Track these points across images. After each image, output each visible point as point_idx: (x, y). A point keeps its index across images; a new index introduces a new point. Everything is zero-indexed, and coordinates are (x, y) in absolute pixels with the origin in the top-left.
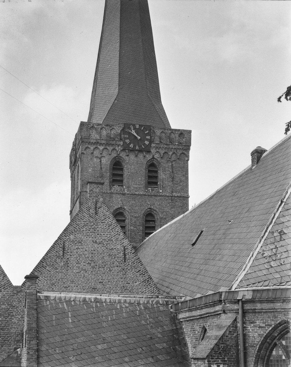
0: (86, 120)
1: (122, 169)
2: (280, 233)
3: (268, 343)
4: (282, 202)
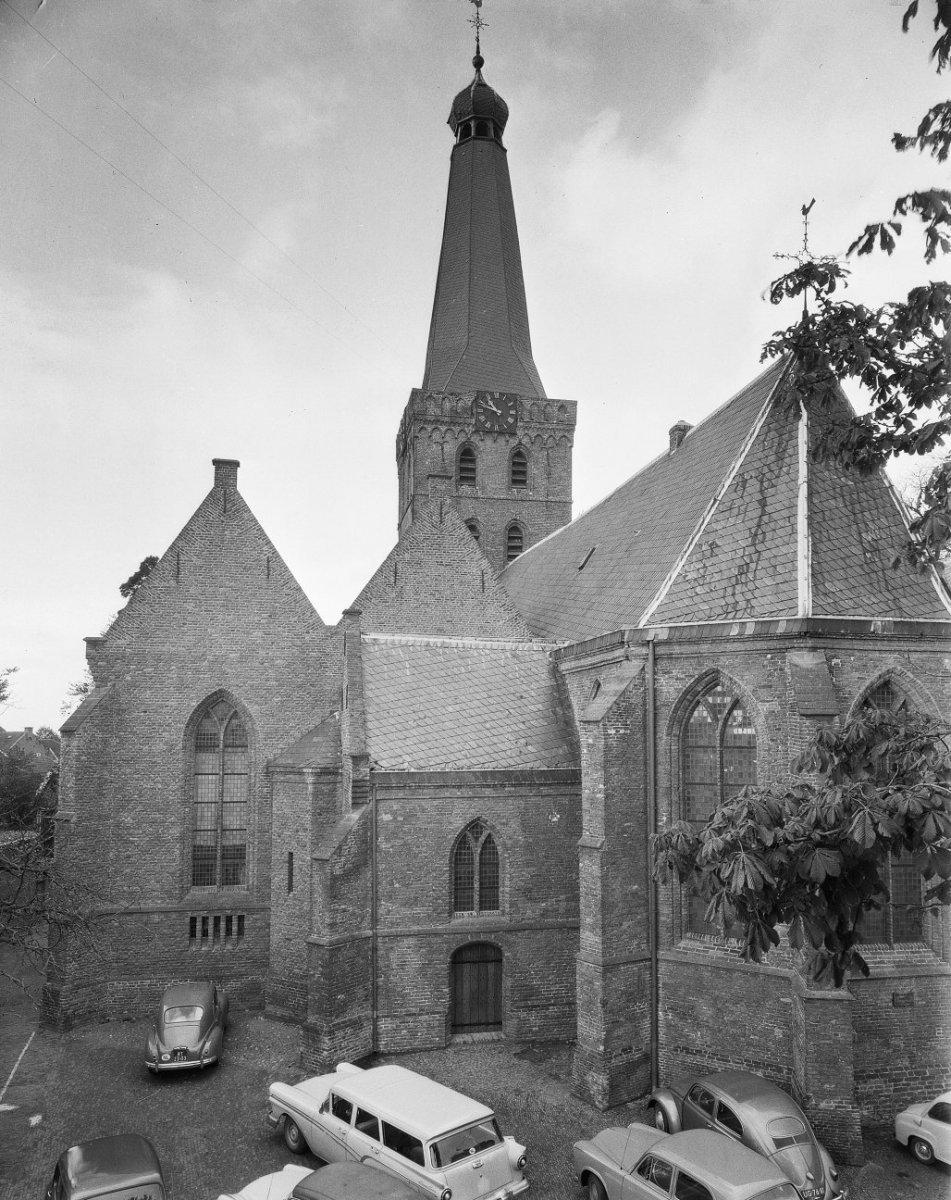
0: (419, 386)
1: (473, 461)
2: (711, 545)
3: (688, 700)
4: (715, 500)
